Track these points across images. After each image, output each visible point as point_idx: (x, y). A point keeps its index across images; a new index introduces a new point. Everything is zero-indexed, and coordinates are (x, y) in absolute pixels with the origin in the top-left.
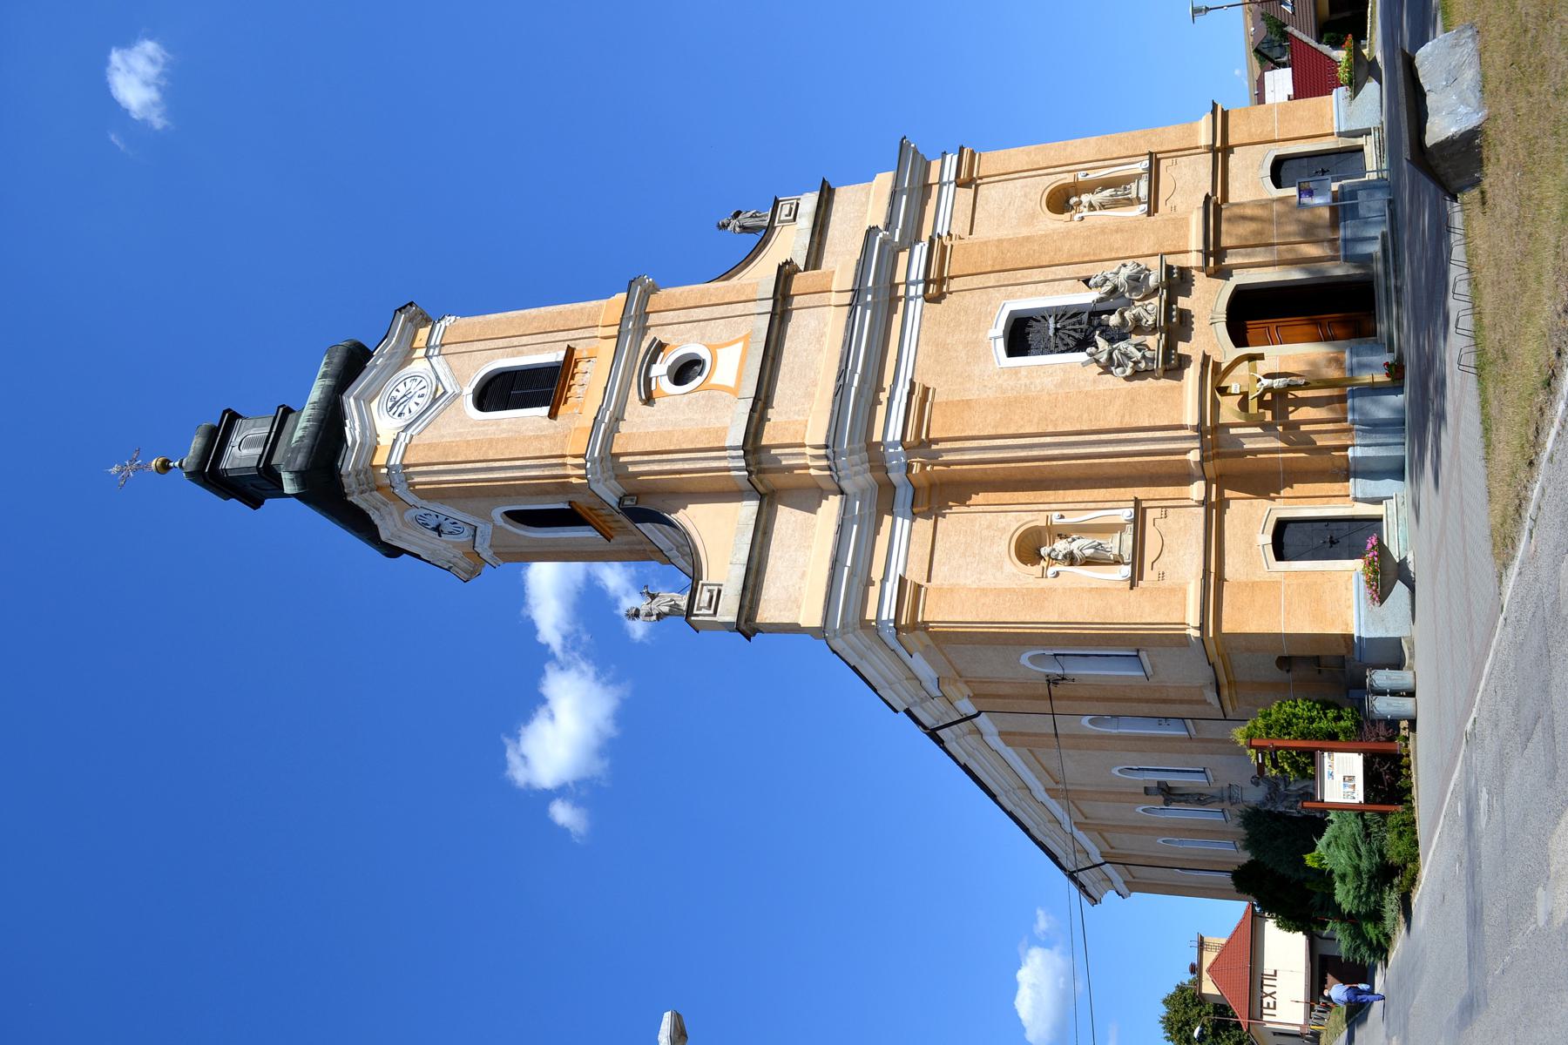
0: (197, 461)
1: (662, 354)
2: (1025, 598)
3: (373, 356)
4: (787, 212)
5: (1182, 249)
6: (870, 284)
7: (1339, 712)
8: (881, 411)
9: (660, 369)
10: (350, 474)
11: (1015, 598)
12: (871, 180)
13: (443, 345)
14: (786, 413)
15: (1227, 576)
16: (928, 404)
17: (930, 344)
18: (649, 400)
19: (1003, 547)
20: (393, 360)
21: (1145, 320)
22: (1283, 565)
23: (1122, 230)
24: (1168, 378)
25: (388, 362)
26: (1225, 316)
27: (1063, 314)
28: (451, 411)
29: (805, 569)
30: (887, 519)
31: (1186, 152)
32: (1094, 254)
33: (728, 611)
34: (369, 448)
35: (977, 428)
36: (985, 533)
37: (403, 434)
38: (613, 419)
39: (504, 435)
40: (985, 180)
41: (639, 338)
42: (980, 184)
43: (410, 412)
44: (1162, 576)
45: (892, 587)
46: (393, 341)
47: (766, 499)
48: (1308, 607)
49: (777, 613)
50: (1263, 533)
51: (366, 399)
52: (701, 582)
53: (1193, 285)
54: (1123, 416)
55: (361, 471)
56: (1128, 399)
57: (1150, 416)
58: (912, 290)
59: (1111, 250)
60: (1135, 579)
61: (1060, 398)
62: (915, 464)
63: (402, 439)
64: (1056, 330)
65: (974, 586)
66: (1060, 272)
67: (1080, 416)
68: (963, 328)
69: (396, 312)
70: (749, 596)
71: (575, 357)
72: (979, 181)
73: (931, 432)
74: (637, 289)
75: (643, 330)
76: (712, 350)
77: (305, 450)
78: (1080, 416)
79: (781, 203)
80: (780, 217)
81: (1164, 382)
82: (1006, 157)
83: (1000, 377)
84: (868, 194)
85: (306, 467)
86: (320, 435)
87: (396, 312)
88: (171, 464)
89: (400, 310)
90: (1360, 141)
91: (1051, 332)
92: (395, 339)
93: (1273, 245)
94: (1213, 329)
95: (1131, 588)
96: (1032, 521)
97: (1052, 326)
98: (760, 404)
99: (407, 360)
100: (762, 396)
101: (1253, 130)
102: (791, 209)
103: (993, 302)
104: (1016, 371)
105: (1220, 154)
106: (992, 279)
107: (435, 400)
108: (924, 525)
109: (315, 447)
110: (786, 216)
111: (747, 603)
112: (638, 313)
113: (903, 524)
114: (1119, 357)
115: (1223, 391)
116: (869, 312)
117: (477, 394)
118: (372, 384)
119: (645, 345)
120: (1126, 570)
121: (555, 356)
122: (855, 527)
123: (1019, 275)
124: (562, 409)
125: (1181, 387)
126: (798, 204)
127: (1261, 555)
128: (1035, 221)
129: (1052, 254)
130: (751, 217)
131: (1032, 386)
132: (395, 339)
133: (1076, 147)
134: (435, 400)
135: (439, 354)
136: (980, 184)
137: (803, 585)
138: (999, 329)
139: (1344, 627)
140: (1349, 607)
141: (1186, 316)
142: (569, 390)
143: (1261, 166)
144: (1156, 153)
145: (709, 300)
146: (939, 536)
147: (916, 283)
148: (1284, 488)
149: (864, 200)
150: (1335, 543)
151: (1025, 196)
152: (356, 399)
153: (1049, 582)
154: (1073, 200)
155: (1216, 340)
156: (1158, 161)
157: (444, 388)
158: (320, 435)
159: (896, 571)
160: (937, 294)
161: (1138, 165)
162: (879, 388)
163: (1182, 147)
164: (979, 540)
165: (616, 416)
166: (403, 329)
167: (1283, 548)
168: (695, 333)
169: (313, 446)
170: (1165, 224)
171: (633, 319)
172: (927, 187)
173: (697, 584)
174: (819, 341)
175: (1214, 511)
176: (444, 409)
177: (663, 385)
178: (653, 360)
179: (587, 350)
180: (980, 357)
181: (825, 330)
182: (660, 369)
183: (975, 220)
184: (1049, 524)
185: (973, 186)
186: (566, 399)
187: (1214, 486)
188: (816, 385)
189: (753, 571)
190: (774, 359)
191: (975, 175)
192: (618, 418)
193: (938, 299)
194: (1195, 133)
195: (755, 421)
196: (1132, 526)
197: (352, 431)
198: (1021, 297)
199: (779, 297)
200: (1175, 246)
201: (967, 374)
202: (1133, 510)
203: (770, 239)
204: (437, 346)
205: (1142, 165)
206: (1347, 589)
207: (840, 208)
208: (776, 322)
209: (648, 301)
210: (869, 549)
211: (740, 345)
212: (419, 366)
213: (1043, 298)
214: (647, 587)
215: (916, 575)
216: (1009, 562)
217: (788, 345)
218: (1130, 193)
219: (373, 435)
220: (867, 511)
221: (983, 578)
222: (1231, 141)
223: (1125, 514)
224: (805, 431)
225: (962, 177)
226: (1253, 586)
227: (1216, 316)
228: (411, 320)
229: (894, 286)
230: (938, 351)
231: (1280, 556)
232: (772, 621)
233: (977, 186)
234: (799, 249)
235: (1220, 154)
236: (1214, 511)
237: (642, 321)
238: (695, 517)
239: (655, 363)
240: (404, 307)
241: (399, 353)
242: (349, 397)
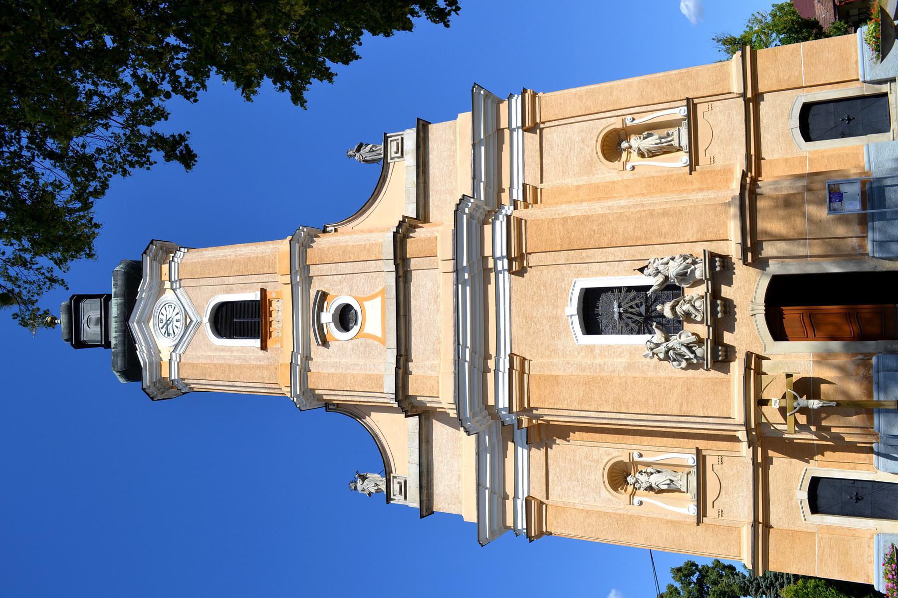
0: (68, 331)
1: (326, 303)
2: (619, 522)
3: (138, 292)
5: (725, 238)
6: (465, 264)
8: (490, 377)
9: (327, 317)
10: (149, 386)
11: (611, 522)
12: (455, 118)
13: (181, 280)
14: (422, 367)
15: (772, 523)
16: (525, 375)
17: (521, 315)
18: (325, 343)
19: (598, 476)
20: (153, 291)
21: (694, 316)
22: (818, 518)
23: (668, 215)
24: (716, 370)
25: (150, 293)
26: (764, 308)
28: (198, 336)
29: (459, 473)
30: (511, 445)
31: (720, 97)
32: (646, 238)
33: (413, 501)
34: (156, 364)
35: (566, 402)
36: (584, 462)
37: (174, 354)
38: (304, 359)
39: (237, 362)
40: (547, 124)
41: (308, 285)
42: (543, 128)
43: (177, 327)
44: (721, 513)
45: (521, 504)
46: (148, 280)
47: (423, 417)
48: (837, 558)
49: (446, 506)
50: (800, 489)
51: (144, 321)
52: (392, 475)
53: (734, 274)
54: (682, 405)
55: (156, 382)
56: (685, 389)
57: (703, 406)
58: (499, 263)
59: (660, 235)
60: (693, 164)
61: (628, 382)
62: (524, 419)
63: (174, 358)
64: (620, 313)
65: (581, 507)
66: (618, 253)
67: (647, 401)
68: (545, 302)
69: (142, 255)
70: (425, 492)
71: (268, 299)
72: (542, 126)
73: (531, 402)
74: (295, 245)
75: (308, 280)
76: (360, 301)
77: (120, 355)
78: (647, 401)
79: (389, 139)
80: (391, 156)
81: (714, 374)
82: (562, 102)
83: (579, 353)
84: (455, 132)
85: (125, 368)
86: (126, 341)
87: (142, 255)
88: (56, 321)
89: (145, 252)
90: (885, 88)
91: (616, 316)
92: (148, 277)
93: (806, 239)
94: (754, 320)
95: (698, 524)
96: (618, 456)
98: (402, 359)
99: (162, 291)
100: (403, 352)
101: (781, 75)
102: (398, 144)
103: (566, 279)
104: (591, 349)
105: (751, 104)
106: (562, 257)
107: (187, 327)
108: (538, 454)
109: (126, 351)
111: (425, 498)
112: (301, 267)
113: (523, 452)
114: (674, 357)
116: (468, 288)
118: (145, 309)
119: (313, 293)
120: (683, 158)
121: (255, 296)
122: (488, 455)
123: (584, 255)
125: (728, 381)
126: (402, 139)
127: (799, 508)
128: (593, 169)
129: (610, 236)
130: (370, 151)
131: (606, 367)
132: (148, 277)
133: (621, 91)
134: (187, 327)
135: (180, 287)
136: (543, 128)
137: (460, 486)
138: (572, 308)
139: (867, 579)
140: (870, 562)
141: (729, 306)
142: (270, 326)
143: (790, 116)
144: (692, 99)
145: (350, 258)
146: (550, 462)
147: (501, 258)
148: (817, 455)
149: (453, 138)
150: (860, 500)
151: (583, 141)
152: (138, 323)
153: (635, 509)
154: (624, 145)
155: (756, 332)
156: (695, 105)
158: (126, 341)
159: (523, 493)
160: (533, 125)
161: (677, 110)
162: (487, 357)
163: (715, 93)
164: (580, 468)
165: (305, 356)
166: (151, 267)
167: (817, 500)
168: (345, 284)
169: (125, 351)
170: (706, 209)
171: (299, 273)
172: (500, 131)
173: (390, 476)
174: (436, 302)
175: (760, 469)
176: (195, 334)
177: (332, 330)
178: (321, 309)
179: (275, 292)
180: (561, 333)
181: (439, 291)
182: (327, 317)
183: (544, 166)
184: (631, 460)
185: (538, 131)
186: (270, 333)
187: (760, 449)
188: (440, 343)
189: (425, 474)
190: (405, 316)
191: (538, 121)
192: (307, 358)
193: (521, 272)
194: (726, 77)
195: (400, 377)
196: (686, 121)
197: (142, 355)
198: (588, 275)
199: (399, 261)
200: (716, 234)
201: (552, 348)
202: (686, 108)
203: (387, 175)
204: (176, 281)
205: (681, 112)
206: (869, 547)
207: (435, 146)
208: (401, 284)
209: (306, 255)
210: (501, 465)
212: (169, 296)
213: (607, 278)
215: (539, 494)
216: (604, 488)
217: (414, 303)
218: (673, 140)
219: (156, 352)
220: (495, 440)
221: (587, 499)
222: (761, 88)
223: (690, 459)
224: (438, 387)
225: (527, 125)
226: (793, 535)
227: (756, 307)
228: (154, 259)
229: (485, 259)
230: (527, 323)
231: (815, 509)
232: (444, 511)
233: (541, 130)
234: (411, 186)
235: (751, 104)
236: (760, 469)
237: (306, 273)
238: (378, 422)
241: (154, 286)
242: (133, 323)
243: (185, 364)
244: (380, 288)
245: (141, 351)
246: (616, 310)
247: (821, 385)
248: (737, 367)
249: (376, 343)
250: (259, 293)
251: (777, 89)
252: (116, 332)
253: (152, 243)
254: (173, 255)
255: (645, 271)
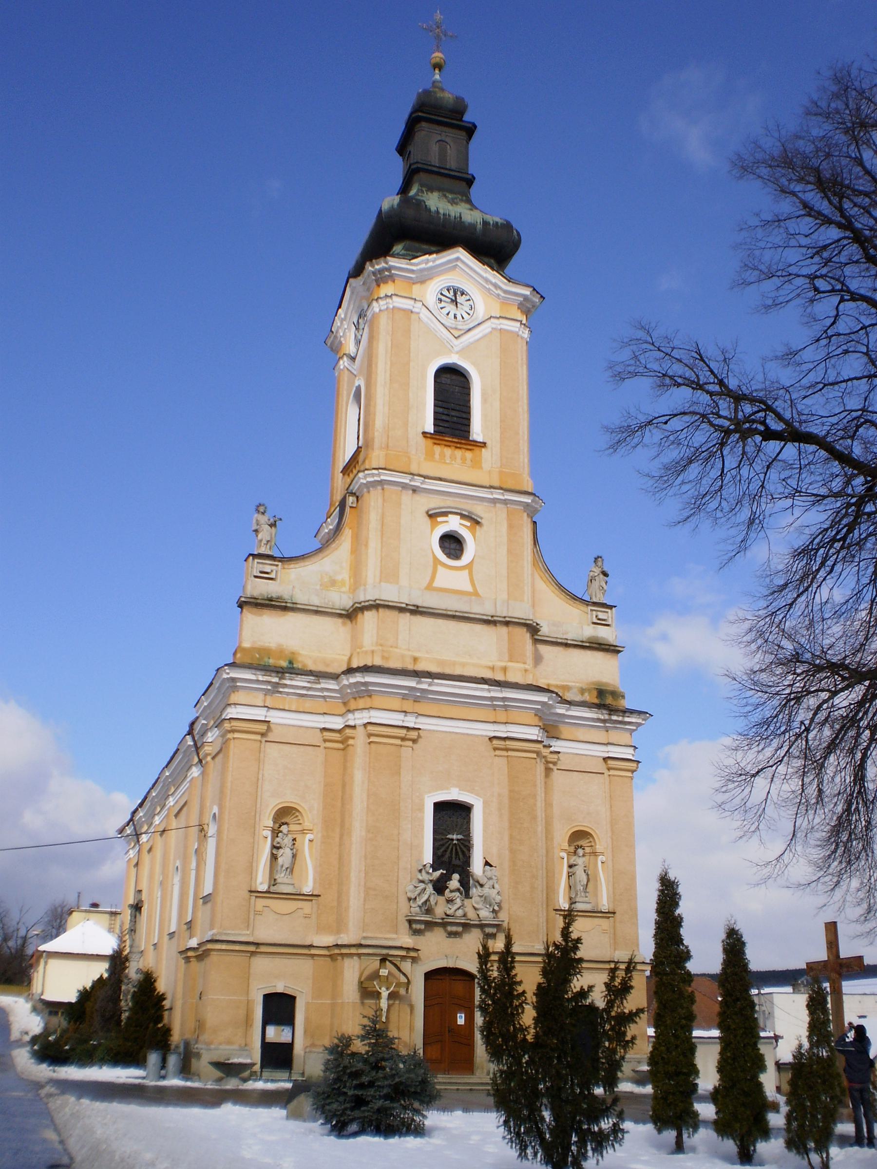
4: (600, 617)
7: (706, 1123)
27: (466, 846)
64: (452, 840)
76: (469, 566)
89: (534, 289)
91: (450, 836)
97: (455, 837)
110: (596, 616)
115: (383, 960)
117: (453, 367)
121: (477, 431)
124: (430, 442)
146: (302, 748)
157: (459, 336)
173: (280, 561)
178: (463, 516)
182: (453, 524)
211: (469, 588)
214: (281, 519)
216: (278, 802)
226: (246, 978)
228: (526, 298)
239: (461, 518)
240: (537, 292)
243: (409, 319)
244: (480, 591)
245: (427, 262)
246: (455, 837)
247: (458, 1023)
248: (407, 940)
249: (428, 579)
250: (480, 438)
251: (172, 753)
252: (444, 214)
253: (542, 297)
254: (524, 322)
255: (488, 867)
